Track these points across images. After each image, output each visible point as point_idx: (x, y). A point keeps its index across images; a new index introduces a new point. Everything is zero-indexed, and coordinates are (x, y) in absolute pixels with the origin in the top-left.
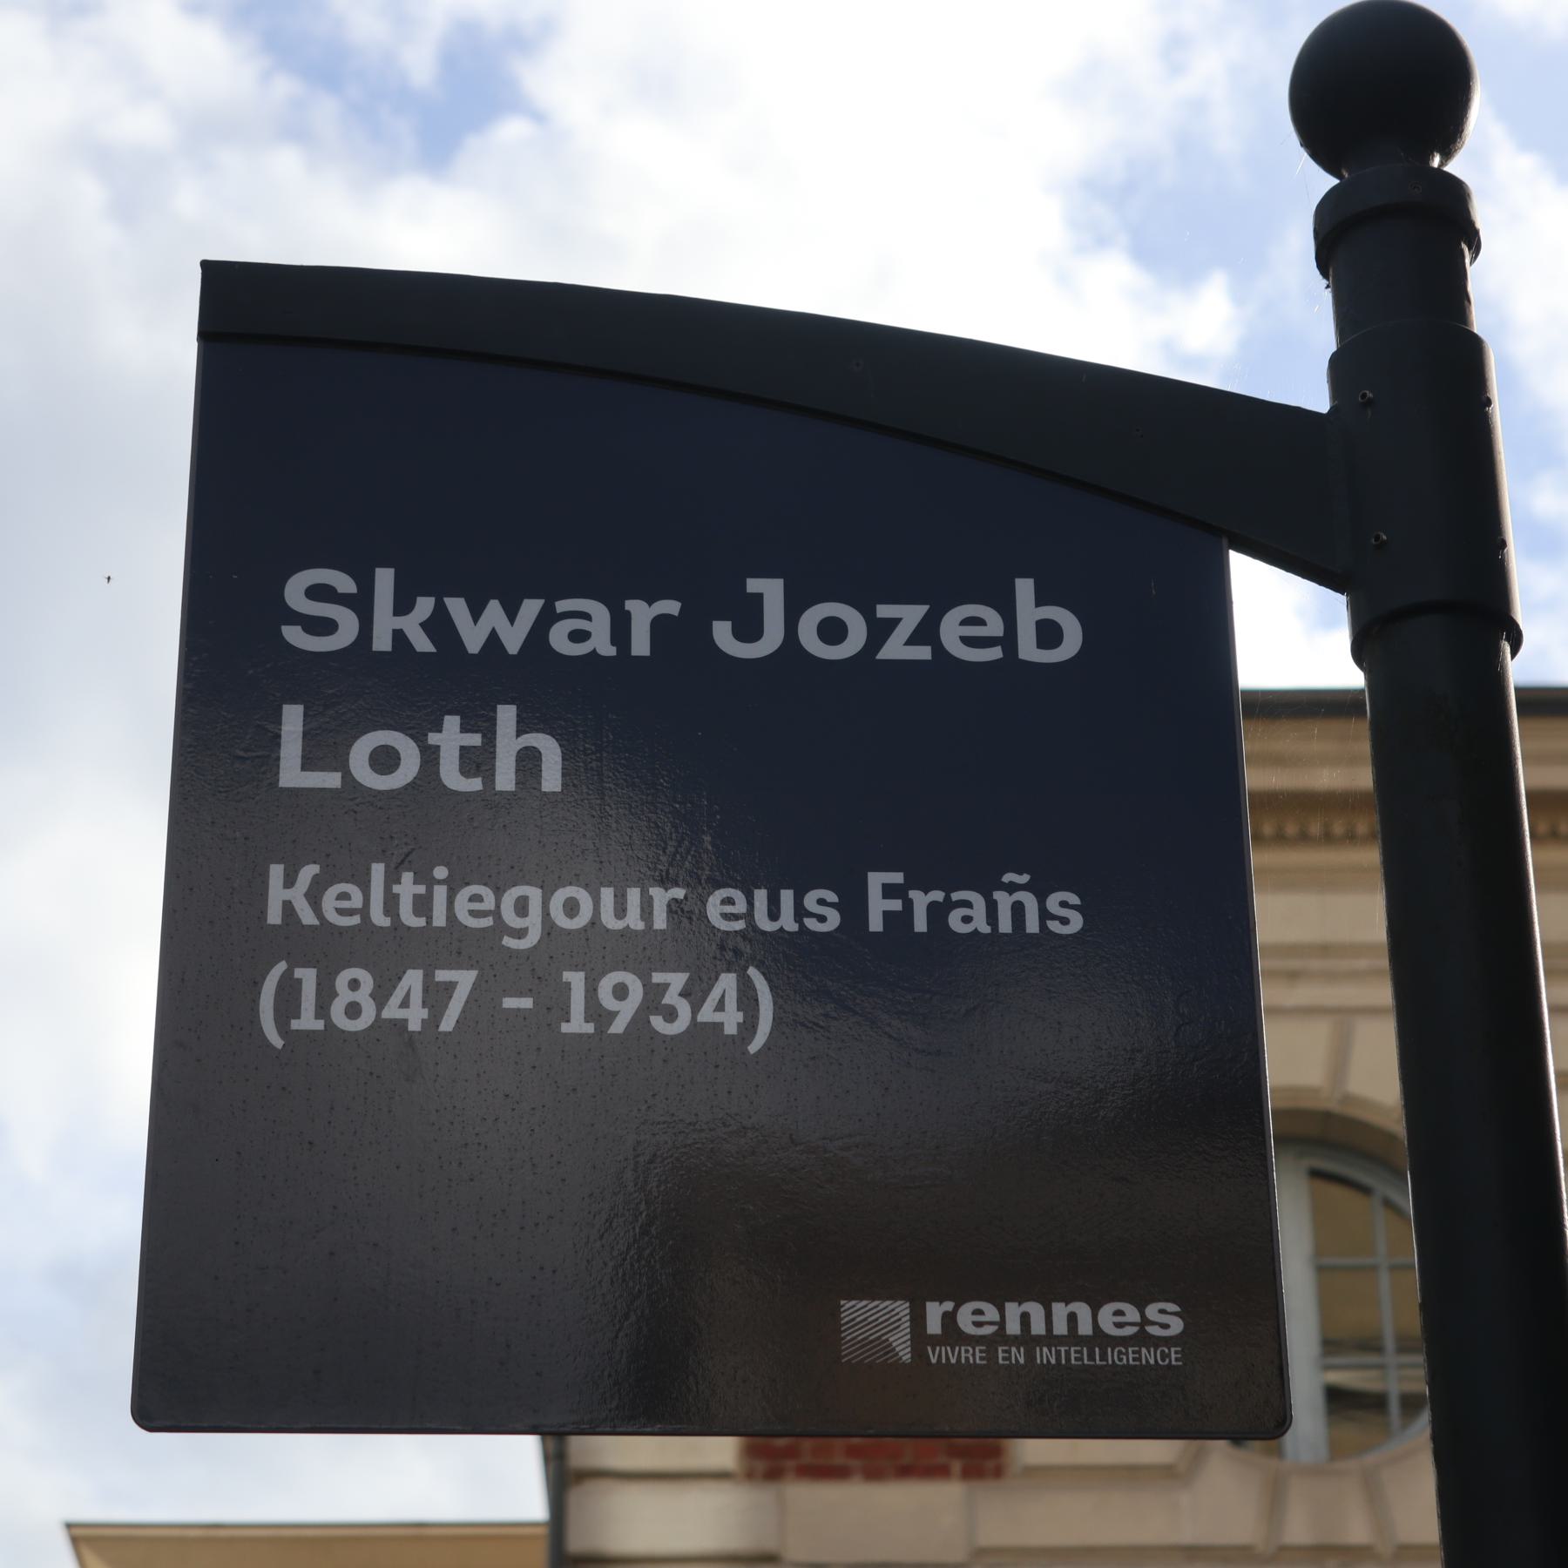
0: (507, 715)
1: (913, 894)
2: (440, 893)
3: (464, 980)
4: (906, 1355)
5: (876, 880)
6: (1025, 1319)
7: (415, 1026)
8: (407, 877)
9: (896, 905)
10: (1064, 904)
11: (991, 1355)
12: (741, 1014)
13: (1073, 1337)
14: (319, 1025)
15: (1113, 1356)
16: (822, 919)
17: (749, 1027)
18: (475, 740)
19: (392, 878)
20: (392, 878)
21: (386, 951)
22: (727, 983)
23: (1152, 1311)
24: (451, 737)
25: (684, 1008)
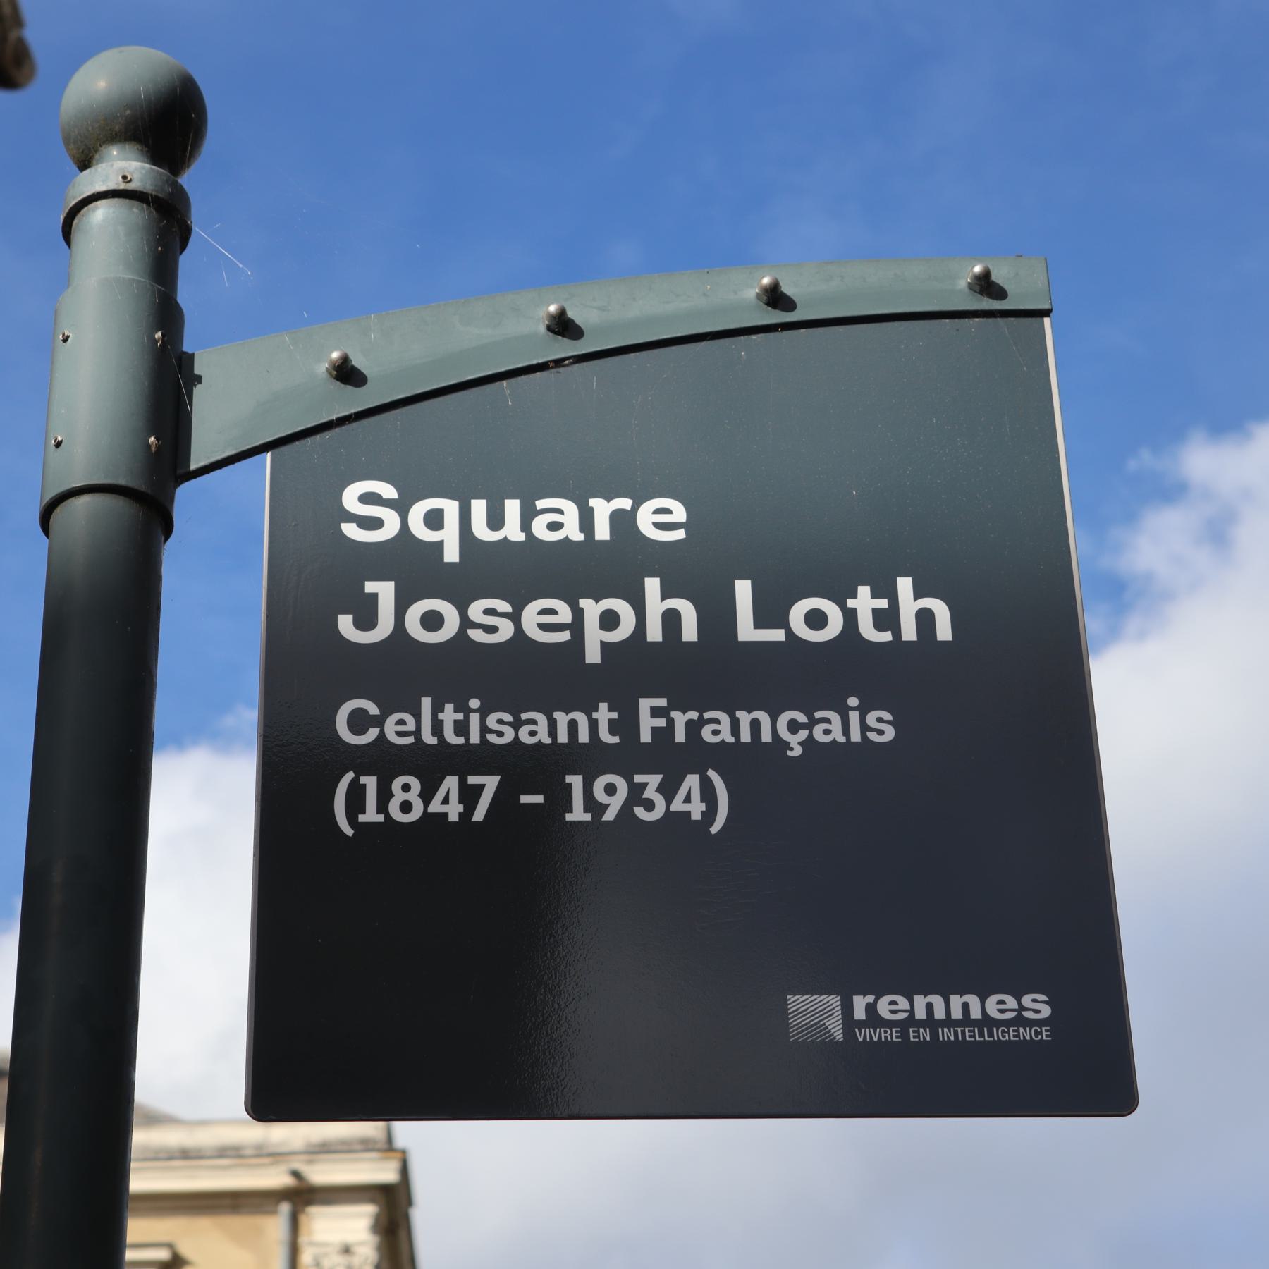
0: (905, 585)
1: (674, 714)
2: (475, 719)
3: (491, 783)
4: (839, 1036)
5: (645, 704)
6: (930, 1007)
7: (454, 818)
8: (449, 707)
9: (661, 722)
10: (880, 720)
11: (904, 1035)
12: (462, 806)
13: (966, 1020)
14: (381, 818)
15: (998, 1034)
16: (881, 732)
17: (710, 814)
18: (883, 603)
19: (437, 708)
20: (437, 708)
21: (431, 764)
22: (692, 782)
23: (1027, 1000)
24: (865, 602)
25: (659, 801)
